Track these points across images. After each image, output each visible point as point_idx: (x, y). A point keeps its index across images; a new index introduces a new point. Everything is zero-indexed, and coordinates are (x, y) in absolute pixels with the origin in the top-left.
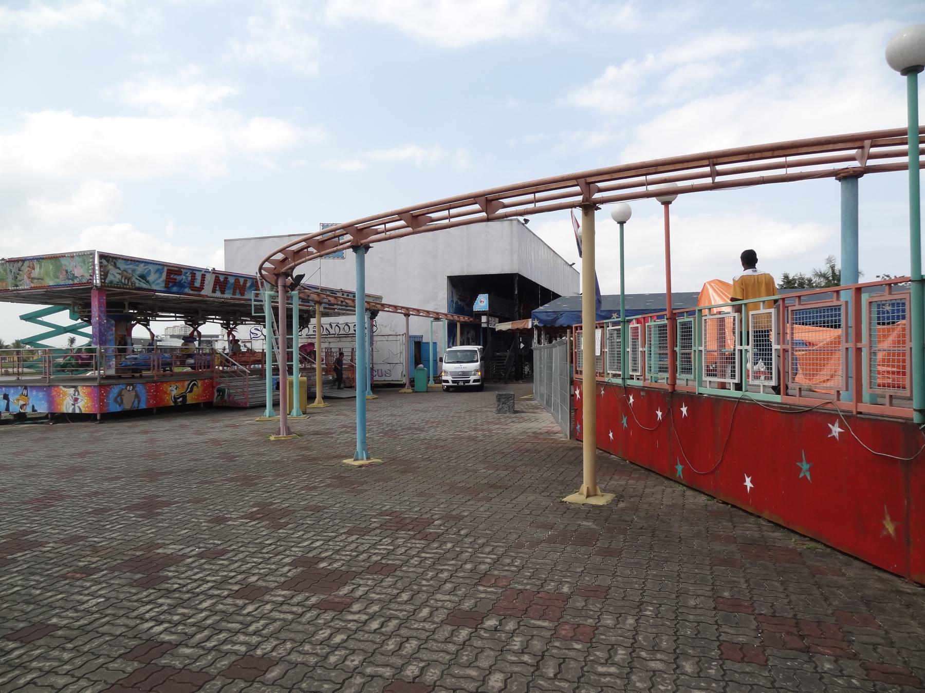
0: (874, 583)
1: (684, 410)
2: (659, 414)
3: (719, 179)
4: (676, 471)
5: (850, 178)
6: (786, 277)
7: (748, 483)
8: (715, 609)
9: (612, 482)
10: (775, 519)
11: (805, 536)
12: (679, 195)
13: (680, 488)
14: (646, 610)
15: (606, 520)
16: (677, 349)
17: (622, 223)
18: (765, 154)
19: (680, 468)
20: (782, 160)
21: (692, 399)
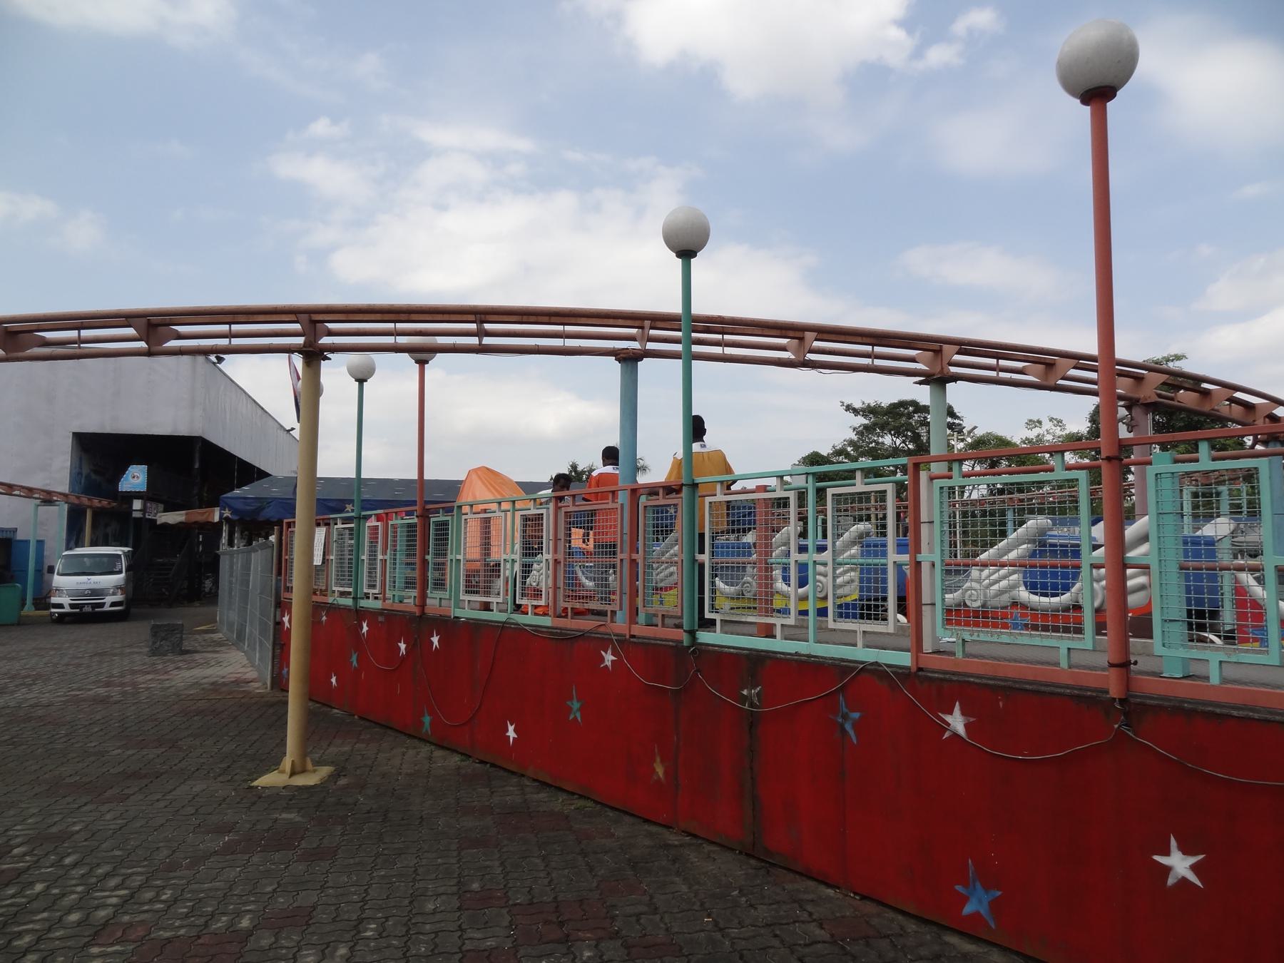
2: (403, 646)
3: (487, 341)
4: (422, 724)
5: (629, 360)
7: (511, 733)
11: (573, 794)
12: (438, 355)
16: (429, 557)
17: (361, 381)
19: (427, 720)
21: (447, 625)
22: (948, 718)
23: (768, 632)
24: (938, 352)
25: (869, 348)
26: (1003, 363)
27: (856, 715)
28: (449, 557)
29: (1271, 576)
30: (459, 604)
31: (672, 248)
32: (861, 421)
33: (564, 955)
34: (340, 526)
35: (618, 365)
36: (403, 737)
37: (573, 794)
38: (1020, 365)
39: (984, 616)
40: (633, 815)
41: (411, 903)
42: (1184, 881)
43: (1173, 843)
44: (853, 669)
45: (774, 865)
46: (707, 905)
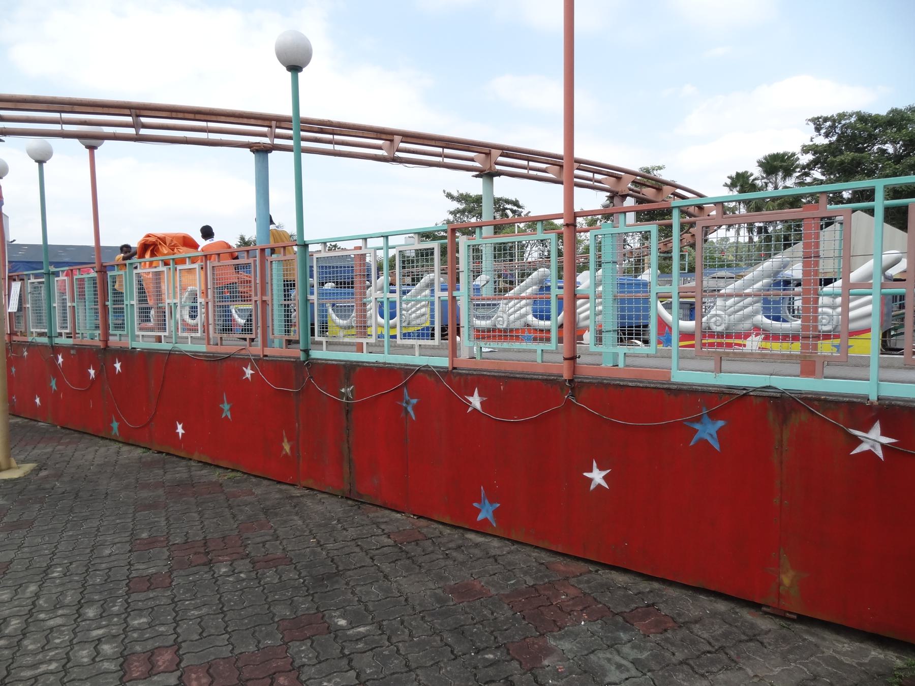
0: (272, 492)
1: (118, 366)
2: (92, 372)
3: (143, 132)
4: (112, 428)
5: (262, 151)
6: (242, 238)
7: (180, 430)
8: (130, 551)
9: (35, 451)
10: (205, 459)
11: (228, 469)
12: (106, 142)
13: (117, 445)
14: (53, 572)
15: (20, 493)
16: (109, 303)
17: (41, 162)
18: (187, 115)
19: (115, 425)
20: (203, 124)
21: (126, 354)
22: (471, 399)
23: (359, 348)
24: (488, 154)
25: (440, 150)
26: (532, 164)
27: (414, 401)
28: (125, 302)
29: (675, 306)
30: (135, 338)
31: (283, 63)
32: (456, 205)
33: (206, 573)
34: (32, 280)
35: (252, 155)
36: (97, 439)
37: (228, 469)
38: (544, 166)
39: (507, 334)
40: (269, 479)
41: (92, 551)
42: (599, 486)
43: (595, 464)
44: (413, 370)
45: (364, 503)
46: (314, 532)
